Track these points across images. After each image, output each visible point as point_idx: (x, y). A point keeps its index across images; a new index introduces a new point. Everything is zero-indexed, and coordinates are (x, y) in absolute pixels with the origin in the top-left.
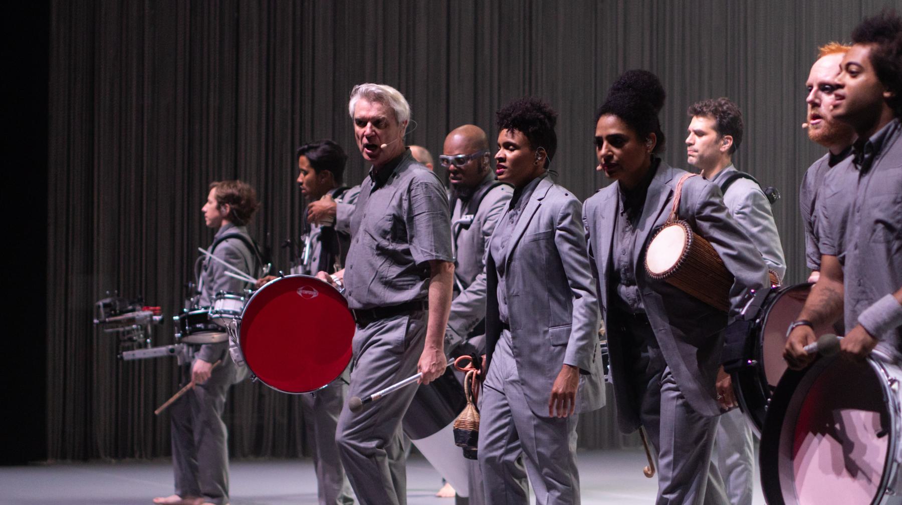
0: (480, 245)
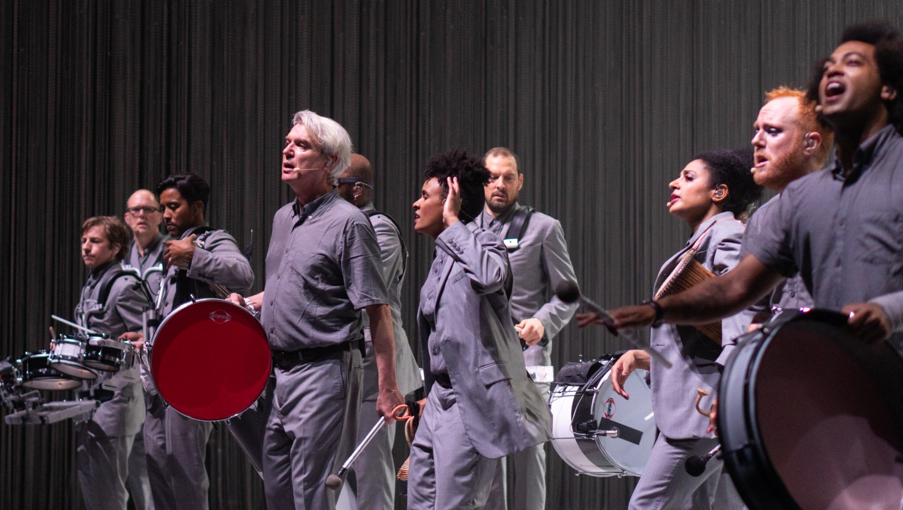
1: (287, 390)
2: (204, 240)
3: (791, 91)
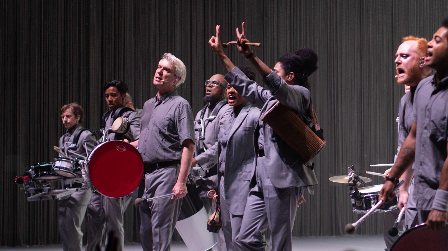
0: (217, 131)
1: (151, 182)
2: (127, 117)
3: (414, 38)
